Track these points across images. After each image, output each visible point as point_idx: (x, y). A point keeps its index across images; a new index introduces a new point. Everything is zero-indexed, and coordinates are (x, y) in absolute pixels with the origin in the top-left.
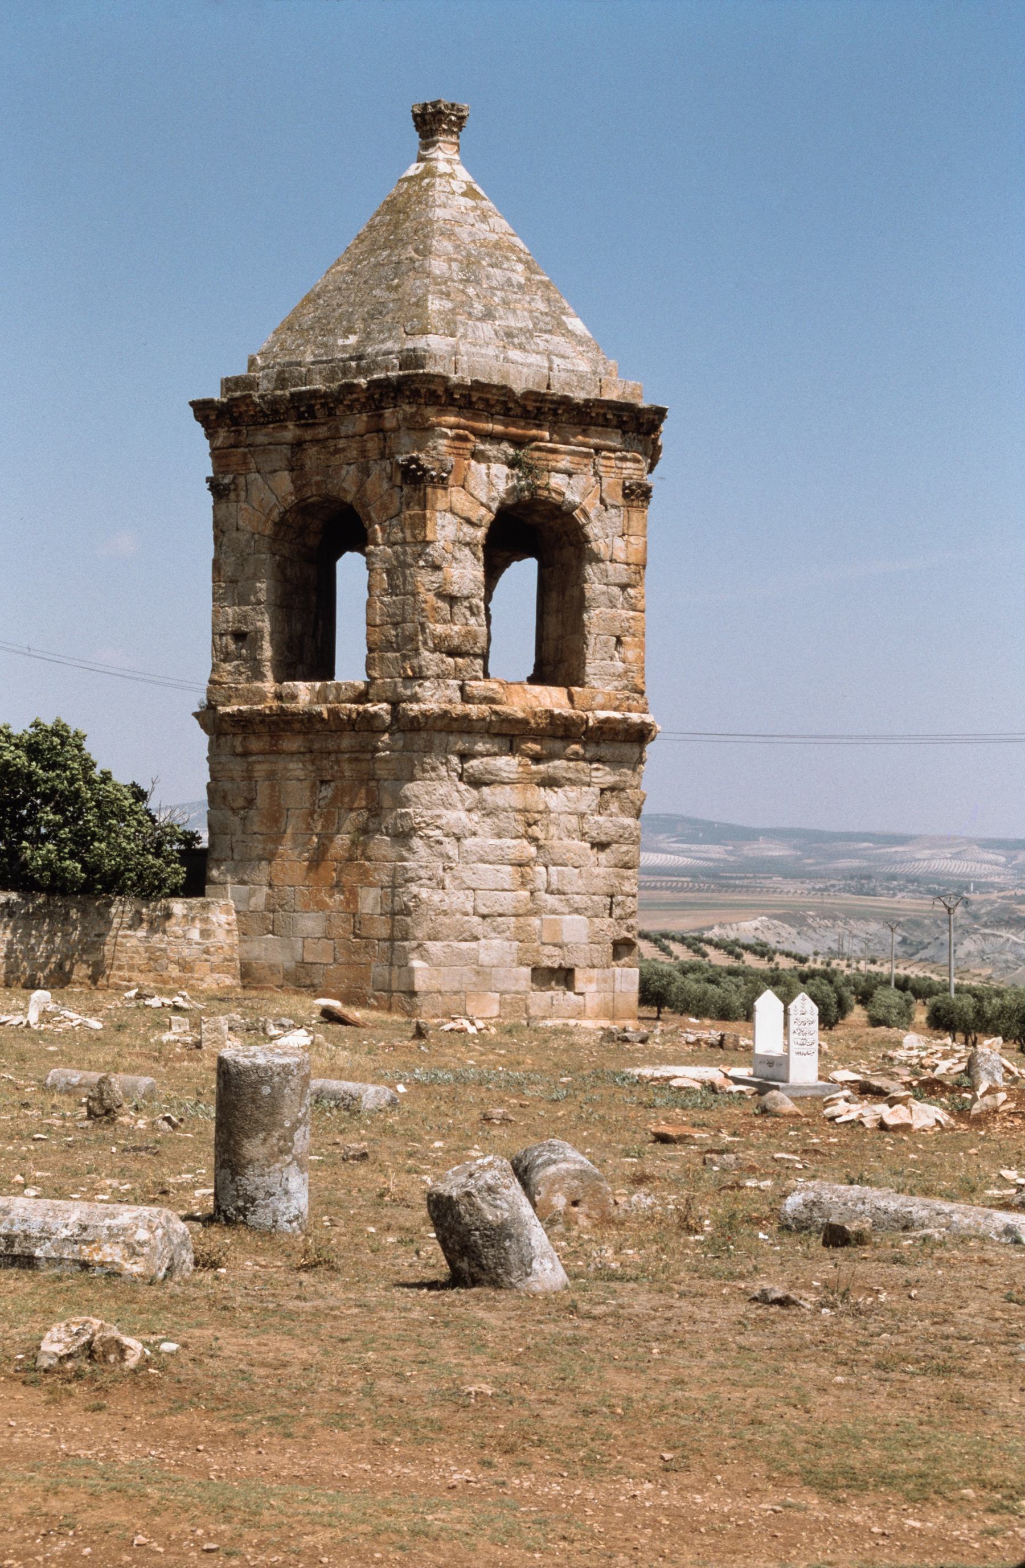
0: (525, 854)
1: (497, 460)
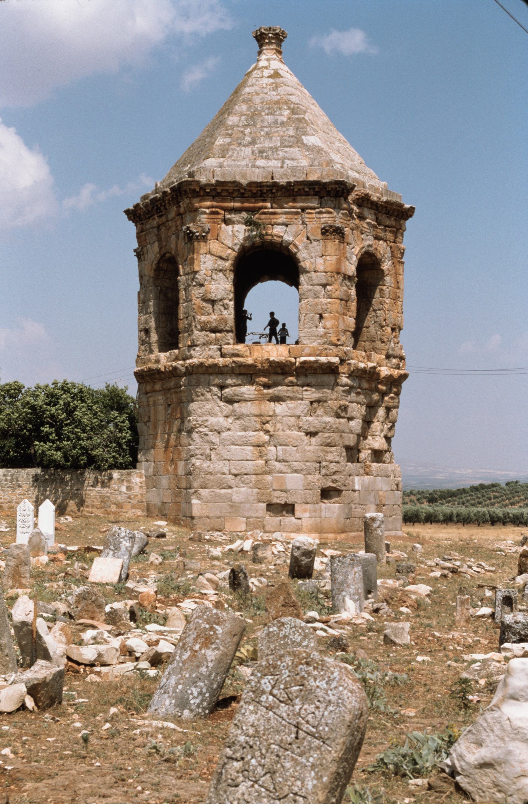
0: (261, 440)
1: (239, 222)
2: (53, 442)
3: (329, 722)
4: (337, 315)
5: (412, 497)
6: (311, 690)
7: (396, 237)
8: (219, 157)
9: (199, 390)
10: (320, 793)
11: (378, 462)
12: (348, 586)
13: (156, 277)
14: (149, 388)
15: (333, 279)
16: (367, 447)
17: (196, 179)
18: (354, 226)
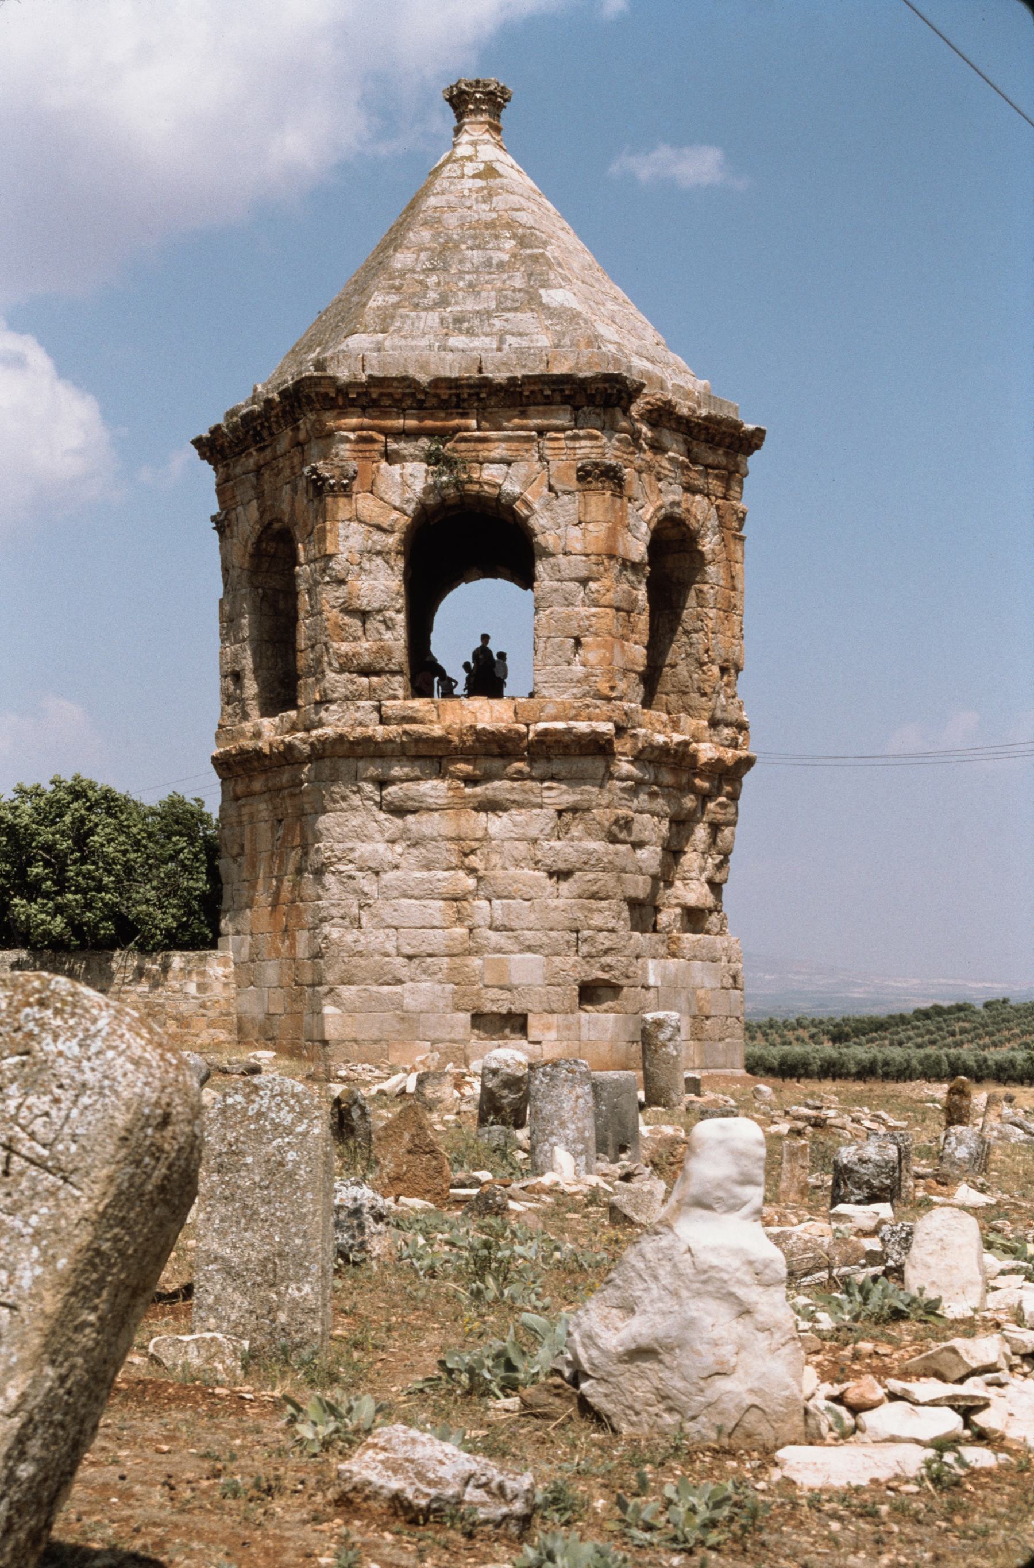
0: (460, 887)
1: (414, 458)
2: (47, 895)
3: (78, 1132)
4: (609, 638)
5: (800, 1032)
6: (46, 1061)
7: (728, 488)
8: (375, 332)
9: (337, 790)
10: (47, 1296)
11: (694, 932)
12: (563, 1124)
13: (255, 570)
14: (240, 789)
15: (602, 568)
16: (674, 901)
17: (330, 372)
18: (642, 463)
